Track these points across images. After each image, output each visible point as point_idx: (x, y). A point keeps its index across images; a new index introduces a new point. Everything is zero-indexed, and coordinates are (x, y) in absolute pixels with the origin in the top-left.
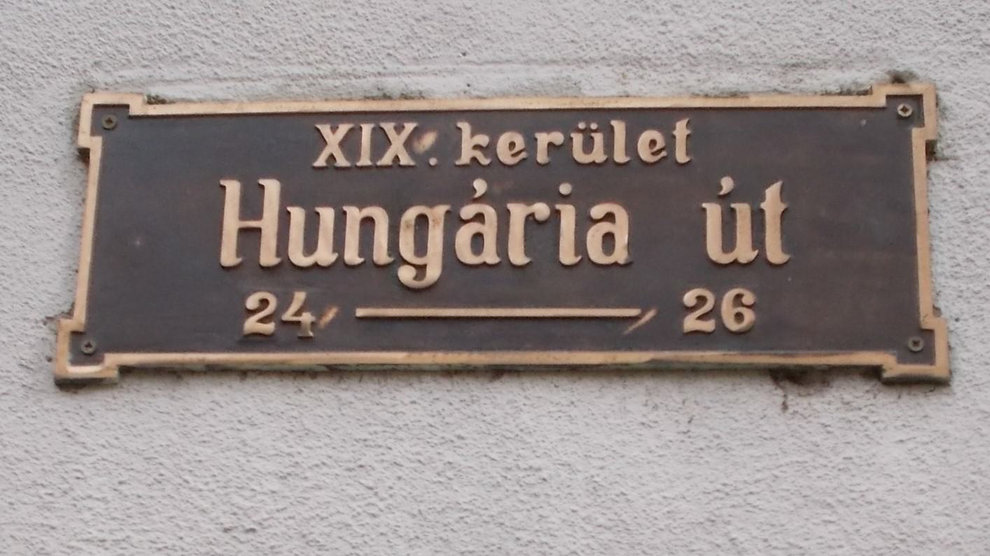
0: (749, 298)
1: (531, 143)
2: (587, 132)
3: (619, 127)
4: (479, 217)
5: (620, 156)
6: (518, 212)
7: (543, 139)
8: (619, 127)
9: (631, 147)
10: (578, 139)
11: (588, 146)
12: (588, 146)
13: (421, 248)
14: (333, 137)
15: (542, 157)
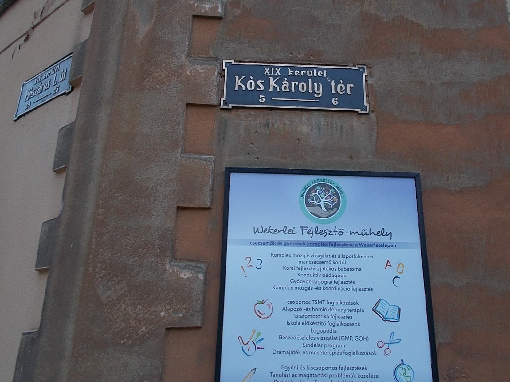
0: (337, 99)
1: (300, 73)
2: (310, 71)
3: (315, 70)
4: (286, 83)
5: (315, 75)
6: (293, 83)
7: (302, 72)
8: (315, 70)
9: (317, 74)
10: (308, 72)
11: (310, 73)
12: (310, 73)
13: (318, 89)
14: (267, 70)
15: (302, 75)
